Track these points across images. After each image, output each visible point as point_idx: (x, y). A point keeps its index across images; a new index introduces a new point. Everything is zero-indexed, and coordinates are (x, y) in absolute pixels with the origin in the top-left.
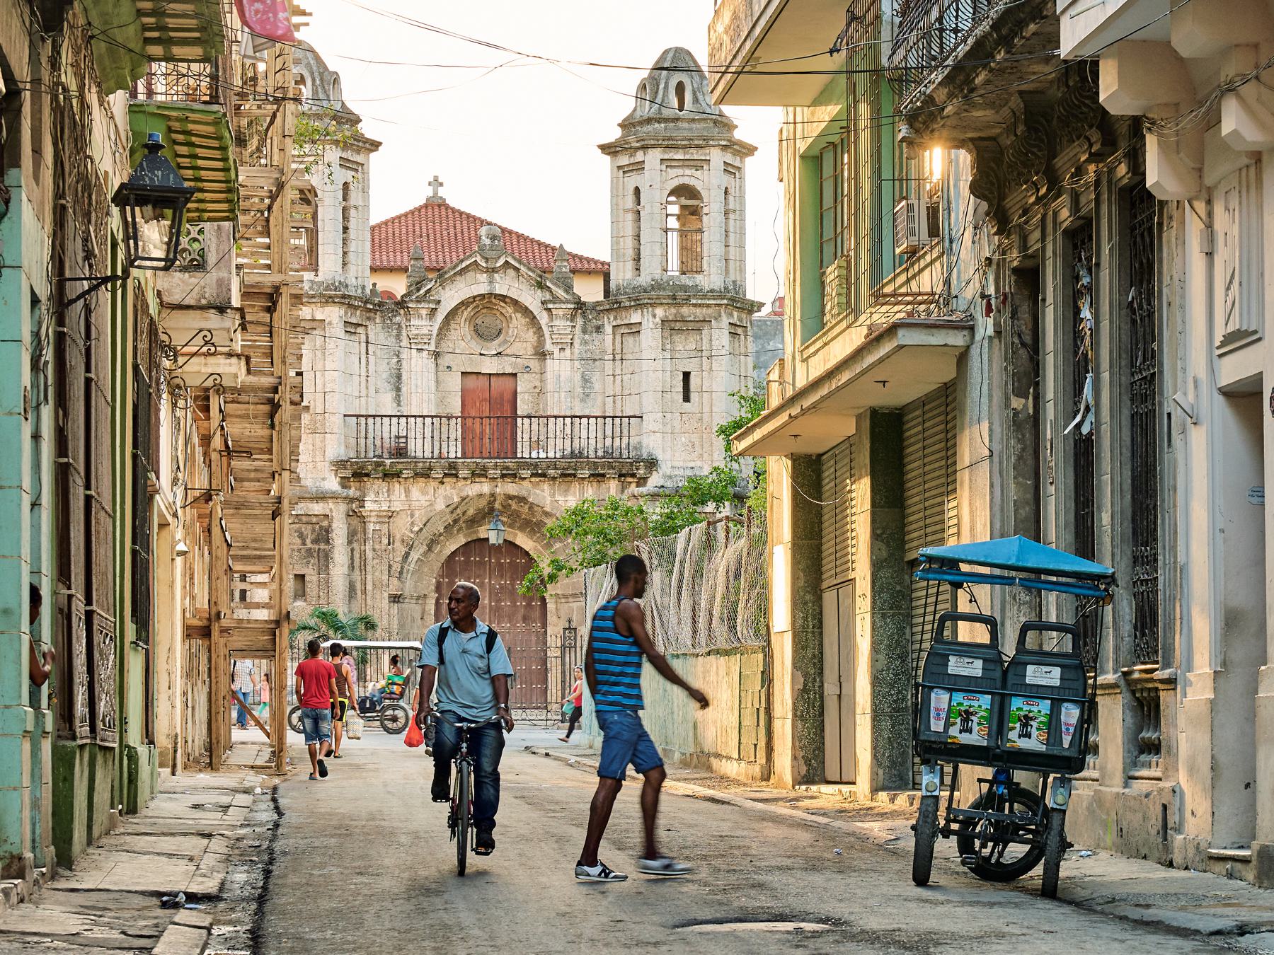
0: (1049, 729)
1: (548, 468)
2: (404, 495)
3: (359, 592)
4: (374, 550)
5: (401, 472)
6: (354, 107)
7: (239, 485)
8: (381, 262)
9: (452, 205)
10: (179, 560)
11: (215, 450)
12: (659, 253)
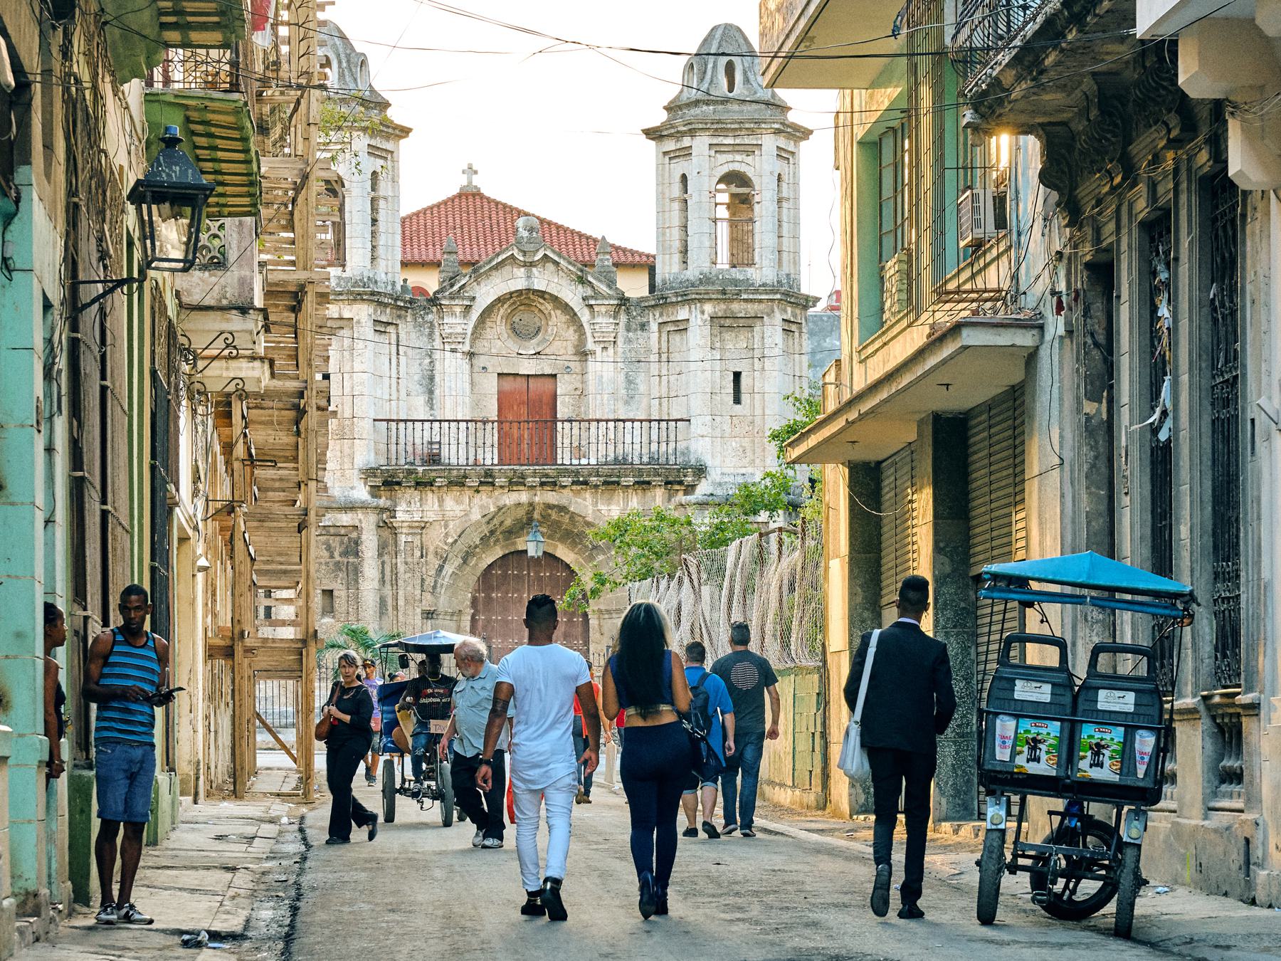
0: (1122, 758)
1: (590, 475)
3: (390, 609)
4: (406, 563)
5: (434, 480)
8: (412, 256)
10: (200, 576)
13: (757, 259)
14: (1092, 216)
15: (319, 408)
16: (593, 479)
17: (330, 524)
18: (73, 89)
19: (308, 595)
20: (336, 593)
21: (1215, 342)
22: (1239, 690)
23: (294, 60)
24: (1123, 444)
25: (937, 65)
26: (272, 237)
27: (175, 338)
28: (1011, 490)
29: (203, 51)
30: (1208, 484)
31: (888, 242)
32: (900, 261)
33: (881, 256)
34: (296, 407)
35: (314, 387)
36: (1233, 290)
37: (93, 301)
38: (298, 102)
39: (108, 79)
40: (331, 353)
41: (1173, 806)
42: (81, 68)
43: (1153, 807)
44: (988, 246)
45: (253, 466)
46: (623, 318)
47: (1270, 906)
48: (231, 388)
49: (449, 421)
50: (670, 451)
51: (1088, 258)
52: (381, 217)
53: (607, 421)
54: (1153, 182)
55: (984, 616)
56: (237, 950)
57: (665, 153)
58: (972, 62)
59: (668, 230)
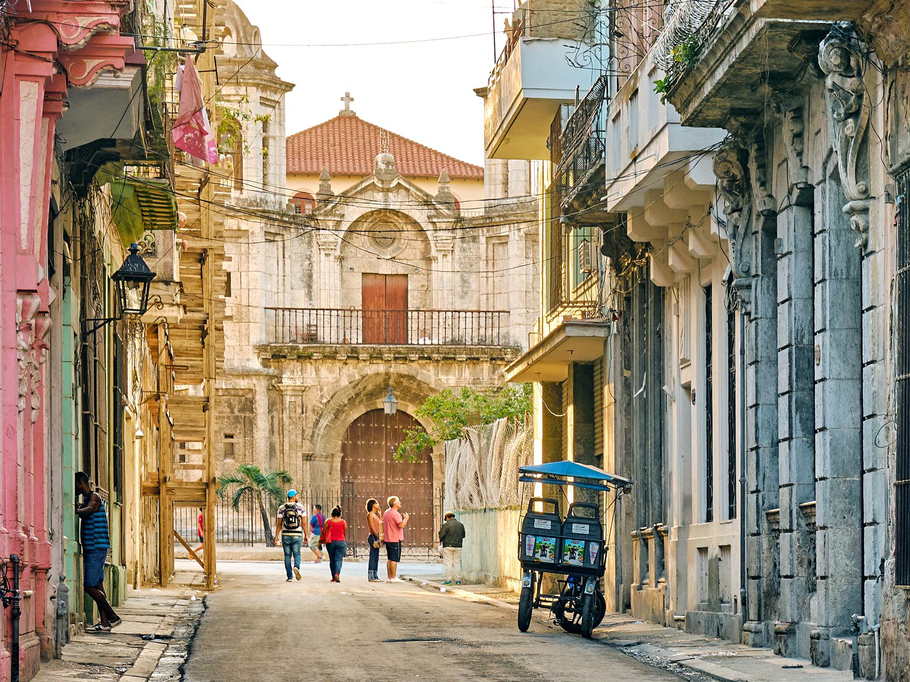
0: (584, 555)
1: (433, 352)
2: (314, 373)
3: (278, 452)
4: (290, 418)
5: (312, 355)
6: (273, 54)
7: (179, 376)
8: (300, 168)
9: (361, 118)
10: (137, 442)
11: (162, 364)
12: (523, 178)
15: (217, 329)
16: (435, 356)
49: (323, 310)
50: (495, 334)
59: (493, 167)
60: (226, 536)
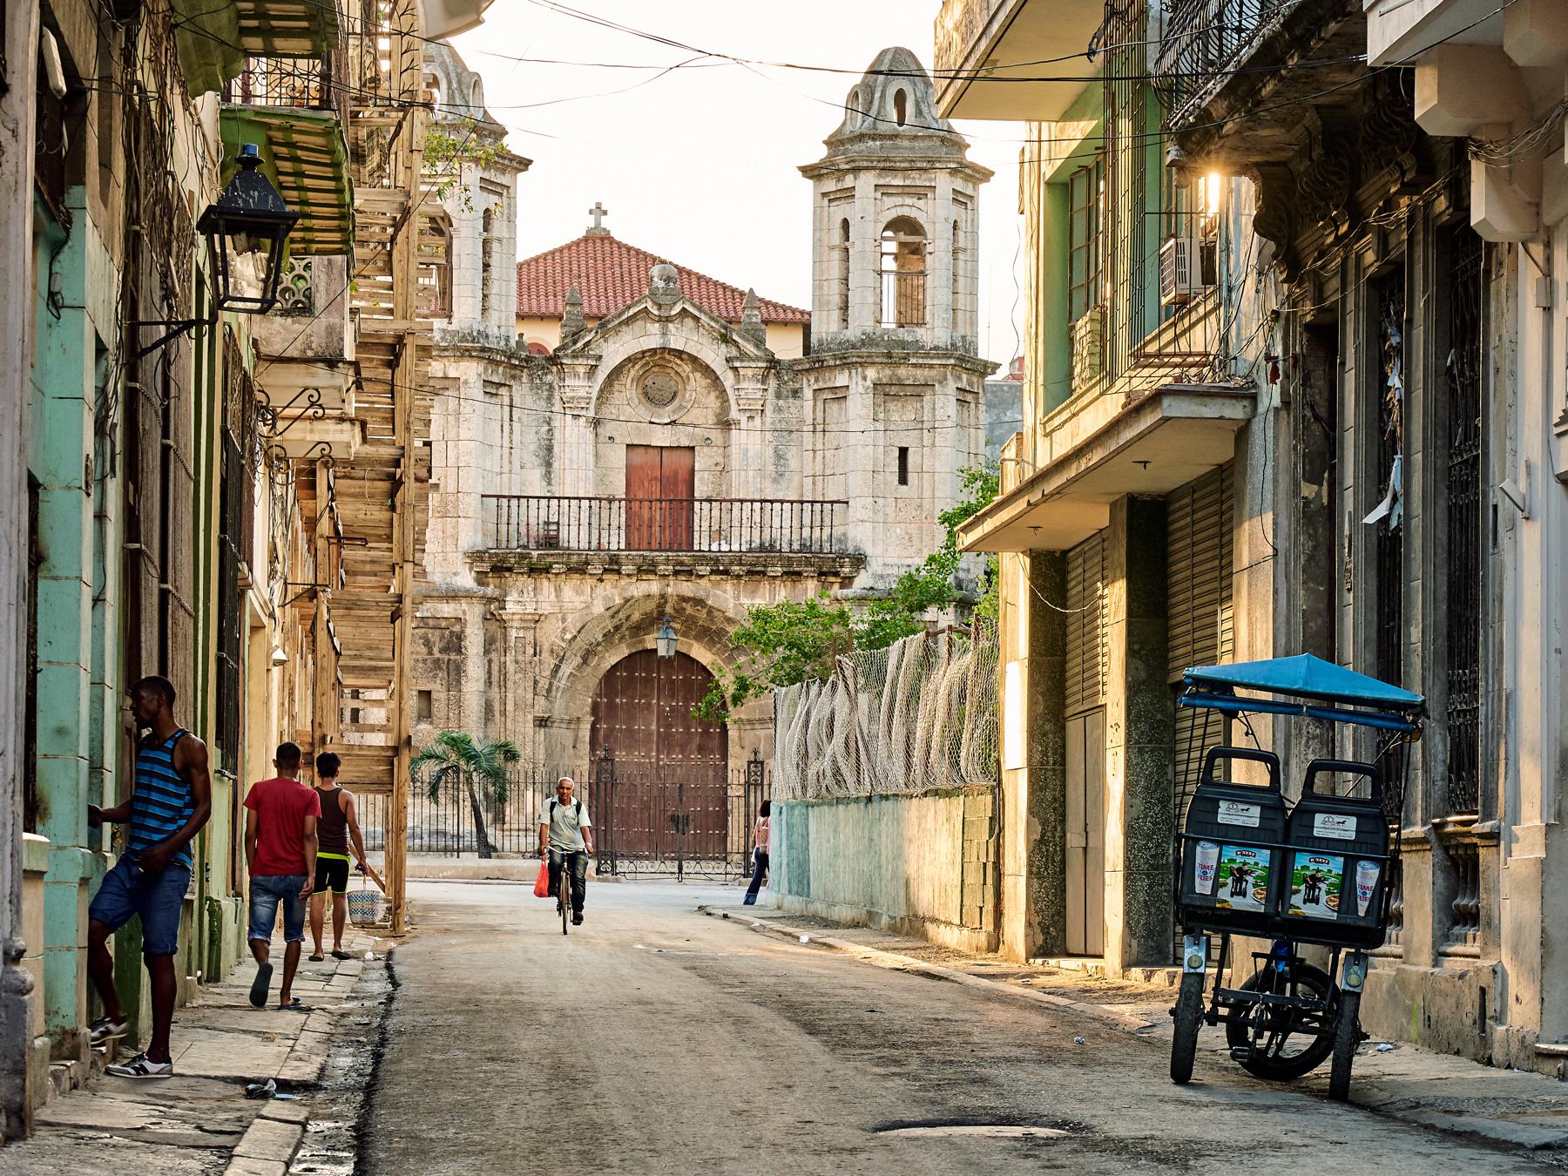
1: (732, 563)
3: (497, 714)
4: (517, 662)
5: (551, 567)
6: (498, 116)
8: (530, 308)
9: (617, 238)
10: (276, 671)
11: (321, 536)
13: (928, 318)
14: (1314, 270)
17: (429, 615)
18: (137, 98)
19: (401, 696)
20: (434, 695)
21: (1453, 416)
22: (1475, 817)
23: (395, 77)
24: (1347, 532)
25: (1139, 94)
26: (367, 280)
27: (251, 393)
28: (1216, 584)
29: (290, 61)
30: (1443, 579)
31: (1079, 298)
32: (1092, 320)
33: (1070, 313)
34: (391, 477)
35: (412, 454)
36: (1474, 357)
37: (156, 345)
38: (400, 126)
39: (177, 90)
40: (432, 417)
41: (1398, 950)
42: (146, 76)
43: (1376, 951)
44: (1193, 304)
45: (340, 545)
46: (772, 383)
47: (1509, 1067)
48: (316, 454)
49: (569, 498)
50: (825, 537)
51: (1308, 318)
52: (495, 261)
53: (752, 501)
54: (1384, 232)
55: (1183, 730)
56: (308, 1102)
57: (824, 195)
58: (1178, 91)
60: (418, 841)
